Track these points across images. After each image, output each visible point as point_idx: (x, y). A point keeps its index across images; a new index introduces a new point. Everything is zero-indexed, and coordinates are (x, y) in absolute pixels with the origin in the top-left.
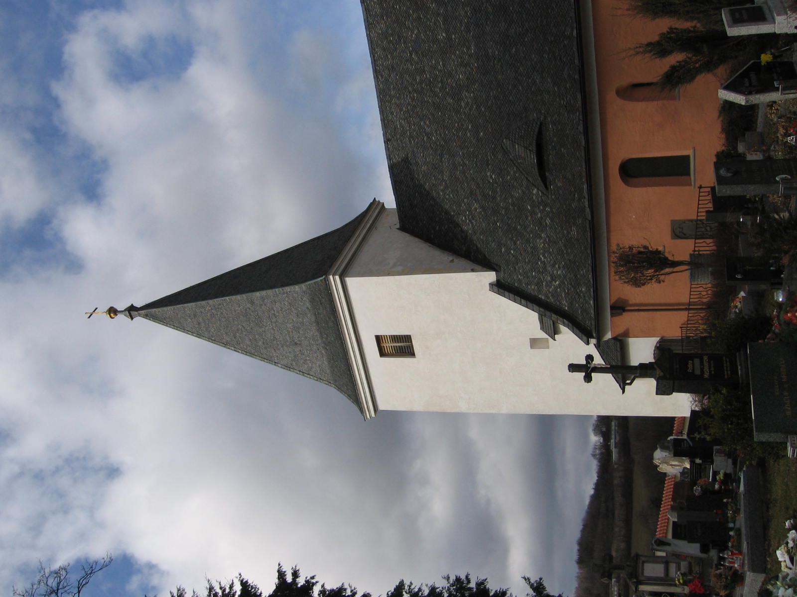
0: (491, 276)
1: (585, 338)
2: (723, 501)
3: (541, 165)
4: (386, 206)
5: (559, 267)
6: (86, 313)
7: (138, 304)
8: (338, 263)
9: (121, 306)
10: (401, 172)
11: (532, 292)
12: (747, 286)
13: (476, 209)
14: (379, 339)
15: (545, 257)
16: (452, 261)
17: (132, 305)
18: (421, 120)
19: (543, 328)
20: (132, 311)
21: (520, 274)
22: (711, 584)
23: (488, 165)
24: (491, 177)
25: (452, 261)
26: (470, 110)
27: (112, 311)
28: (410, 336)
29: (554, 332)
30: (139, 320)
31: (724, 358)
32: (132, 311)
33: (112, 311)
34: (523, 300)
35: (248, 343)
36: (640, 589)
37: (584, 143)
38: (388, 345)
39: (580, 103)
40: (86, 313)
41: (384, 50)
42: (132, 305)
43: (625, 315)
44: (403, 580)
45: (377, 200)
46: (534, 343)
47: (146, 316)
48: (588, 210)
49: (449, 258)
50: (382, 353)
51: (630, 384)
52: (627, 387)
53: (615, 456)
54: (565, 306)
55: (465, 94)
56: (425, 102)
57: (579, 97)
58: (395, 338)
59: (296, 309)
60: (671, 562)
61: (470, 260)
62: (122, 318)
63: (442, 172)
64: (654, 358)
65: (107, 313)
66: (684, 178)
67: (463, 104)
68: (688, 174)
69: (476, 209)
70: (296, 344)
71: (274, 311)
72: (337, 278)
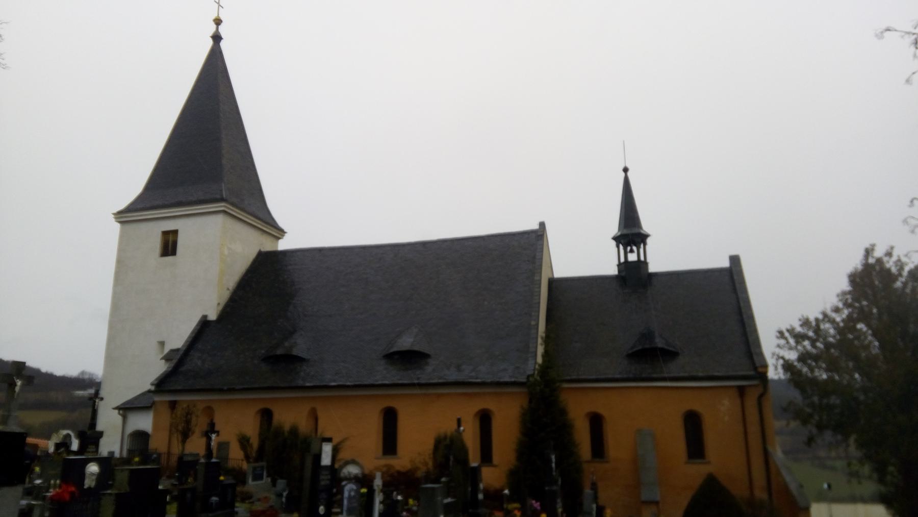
0: (213, 316)
1: (156, 382)
2: (218, 478)
4: (280, 241)
9: (223, 30)
14: (175, 232)
16: (228, 289)
19: (172, 351)
20: (217, 38)
22: (183, 424)
25: (228, 289)
27: (218, 22)
29: (167, 358)
30: (210, 43)
32: (217, 38)
33: (218, 22)
38: (171, 238)
46: (162, 344)
50: (166, 234)
51: (119, 414)
52: (117, 411)
53: (80, 393)
54: (183, 369)
58: (175, 244)
62: (212, 28)
64: (852, 287)
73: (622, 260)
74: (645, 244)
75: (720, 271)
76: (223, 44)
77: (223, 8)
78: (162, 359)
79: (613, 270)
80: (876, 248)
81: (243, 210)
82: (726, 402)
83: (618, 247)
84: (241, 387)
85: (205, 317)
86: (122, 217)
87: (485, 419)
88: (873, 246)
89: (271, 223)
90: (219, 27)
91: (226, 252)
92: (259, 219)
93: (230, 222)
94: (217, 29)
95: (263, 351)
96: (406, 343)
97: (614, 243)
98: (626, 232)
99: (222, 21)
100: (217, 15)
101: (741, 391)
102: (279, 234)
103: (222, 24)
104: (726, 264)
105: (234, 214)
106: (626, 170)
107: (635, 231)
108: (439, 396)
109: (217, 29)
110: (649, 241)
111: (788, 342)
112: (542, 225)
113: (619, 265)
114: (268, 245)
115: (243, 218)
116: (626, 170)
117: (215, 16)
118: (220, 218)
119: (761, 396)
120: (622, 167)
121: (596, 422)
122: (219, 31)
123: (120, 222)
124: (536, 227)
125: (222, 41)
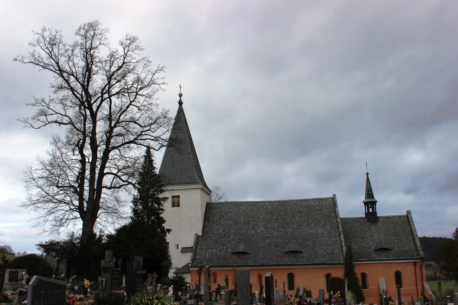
0: (200, 234)
3: (238, 253)
5: (209, 256)
7: (183, 105)
10: (226, 206)
12: (272, 297)
13: (220, 231)
15: (211, 252)
18: (244, 216)
20: (181, 103)
21: (203, 243)
23: (235, 236)
26: (249, 232)
27: (181, 95)
32: (181, 103)
33: (181, 95)
39: (258, 264)
41: (263, 206)
55: (254, 231)
56: (250, 218)
57: (259, 264)
66: (327, 291)
67: (251, 230)
68: (289, 290)
69: (220, 231)
71: (186, 161)
72: (201, 187)
74: (376, 205)
75: (330, 198)
76: (183, 106)
78: (409, 212)
79: (364, 216)
80: (82, 62)
81: (172, 184)
84: (186, 272)
85: (196, 235)
88: (35, 50)
90: (181, 97)
97: (363, 204)
99: (182, 95)
101: (415, 263)
104: (405, 214)
105: (208, 192)
106: (367, 174)
107: (373, 200)
110: (377, 203)
112: (334, 195)
113: (366, 213)
115: (205, 190)
116: (367, 174)
117: (179, 93)
120: (366, 173)
121: (364, 276)
122: (181, 99)
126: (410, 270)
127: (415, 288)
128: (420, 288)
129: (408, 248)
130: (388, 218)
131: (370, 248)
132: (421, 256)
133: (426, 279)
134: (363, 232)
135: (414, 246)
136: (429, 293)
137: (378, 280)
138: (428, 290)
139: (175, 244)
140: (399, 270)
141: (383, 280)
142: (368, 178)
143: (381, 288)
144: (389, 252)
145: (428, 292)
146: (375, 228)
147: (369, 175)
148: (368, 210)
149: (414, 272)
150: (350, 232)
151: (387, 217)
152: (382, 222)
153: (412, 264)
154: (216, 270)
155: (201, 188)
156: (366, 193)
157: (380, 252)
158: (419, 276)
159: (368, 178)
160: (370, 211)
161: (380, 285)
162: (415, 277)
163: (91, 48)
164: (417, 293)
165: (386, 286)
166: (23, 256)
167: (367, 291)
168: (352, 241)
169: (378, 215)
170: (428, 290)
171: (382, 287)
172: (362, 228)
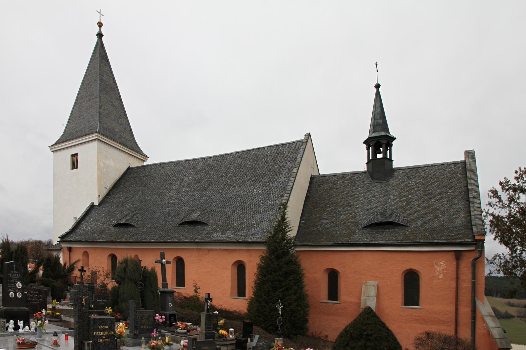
0: (96, 204)
2: (249, 338)
6: (100, 10)
7: (103, 39)
8: (107, 139)
11: (86, 219)
17: (103, 36)
20: (100, 35)
24: (128, 206)
27: (100, 25)
28: (77, 168)
30: (96, 39)
31: (106, 301)
32: (100, 35)
33: (100, 25)
34: (83, 215)
35: (82, 95)
36: (34, 265)
37: (118, 240)
40: (100, 10)
42: (103, 36)
43: (68, 252)
44: (500, 181)
45: (148, 158)
47: (97, 43)
48: (98, 240)
49: (108, 187)
59: (91, 118)
60: (39, 276)
61: (106, 195)
63: (139, 186)
65: (99, 22)
68: (177, 286)
70: (79, 117)
72: (96, 137)
73: (371, 158)
77: (103, 16)
79: (363, 168)
81: (114, 140)
82: (443, 264)
83: (368, 149)
86: (53, 148)
87: (240, 267)
89: (139, 151)
90: (101, 28)
91: (102, 165)
92: (127, 147)
93: (103, 146)
94: (100, 30)
95: (115, 222)
96: (194, 216)
97: (365, 146)
98: (374, 135)
100: (99, 20)
101: (458, 255)
102: (145, 159)
103: (102, 27)
105: (131, 153)
106: (378, 86)
108: (209, 250)
109: (100, 30)
111: (500, 201)
114: (135, 163)
116: (378, 86)
117: (98, 21)
118: (96, 143)
119: (476, 259)
123: (53, 151)
124: (302, 138)
125: (103, 37)
126: (443, 270)
127: (452, 308)
128: (465, 310)
129: (447, 223)
130: (417, 169)
131: (355, 224)
132: (477, 238)
133: (486, 289)
134: (351, 196)
135: (466, 218)
136: (487, 324)
137: (362, 285)
138: (486, 316)
139: (74, 218)
140: (415, 266)
141: (374, 286)
142: (378, 94)
143: (362, 301)
144: (396, 230)
145: (484, 321)
146: (380, 188)
147: (380, 89)
148: (374, 155)
149: (455, 273)
150: (326, 197)
151: (414, 168)
152: (399, 177)
153: (451, 257)
154: (87, 248)
155: (97, 139)
156: (372, 125)
157: (377, 230)
158: (466, 285)
159: (378, 94)
160: (393, 167)
161: (362, 294)
162: (454, 285)
163: (308, 136)
164: (454, 321)
165: (375, 298)
166: (15, 242)
167: (337, 305)
168: (324, 211)
169: (396, 165)
170: (486, 316)
171: (366, 299)
172: (353, 189)
